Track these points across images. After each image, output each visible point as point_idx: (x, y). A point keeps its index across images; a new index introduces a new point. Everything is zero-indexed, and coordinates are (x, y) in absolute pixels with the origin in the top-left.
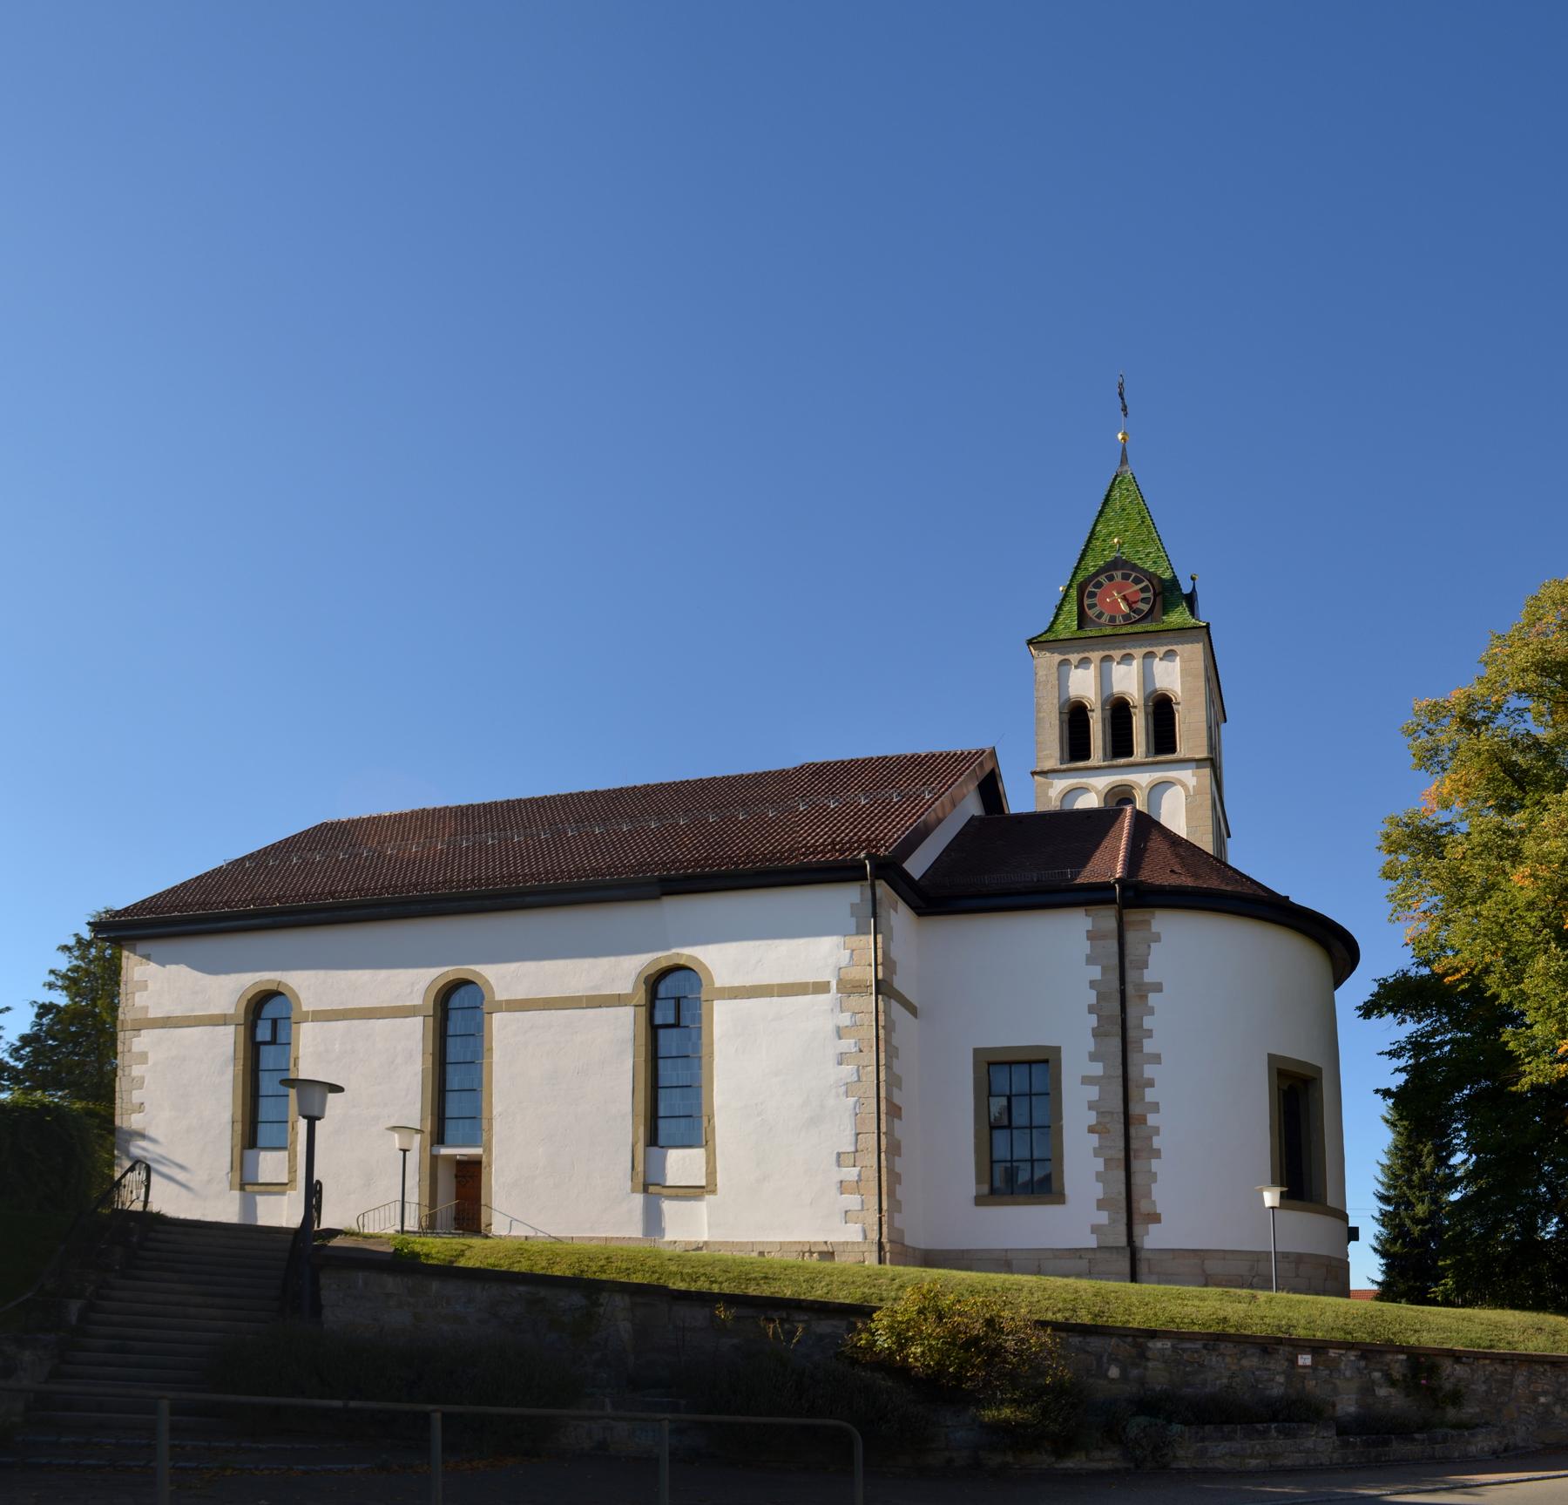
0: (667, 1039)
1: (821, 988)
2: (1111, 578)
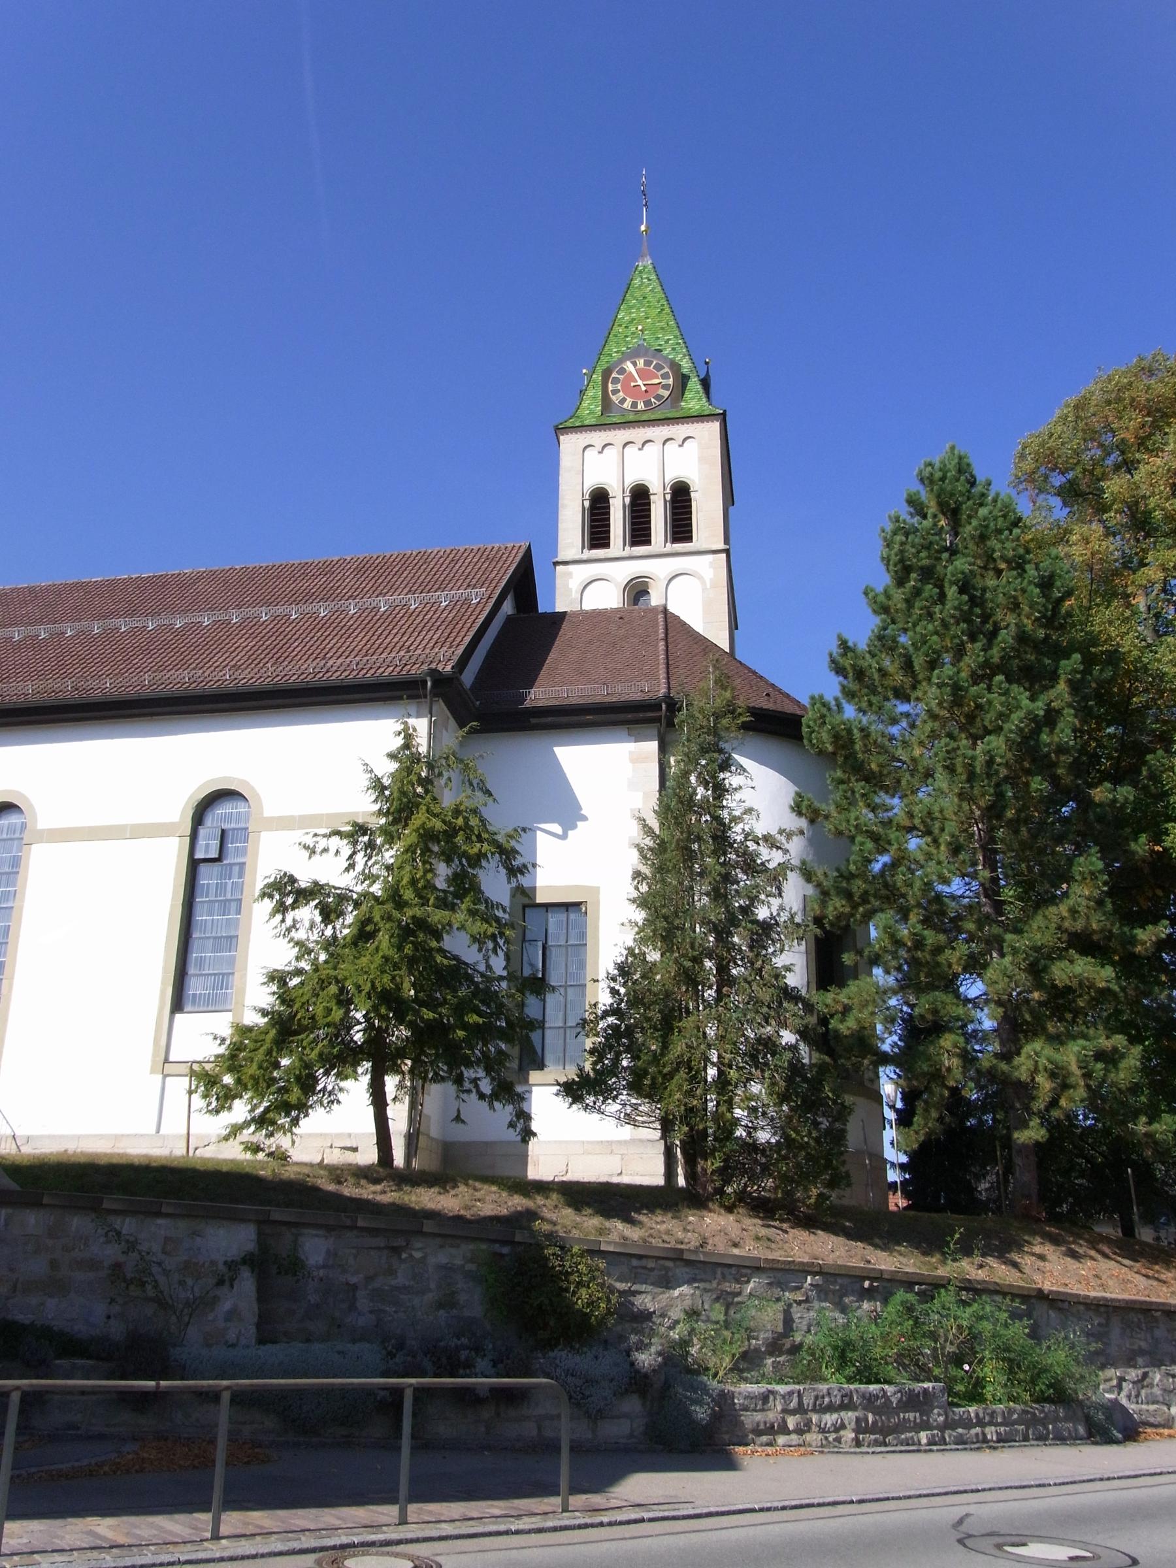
0: (208, 877)
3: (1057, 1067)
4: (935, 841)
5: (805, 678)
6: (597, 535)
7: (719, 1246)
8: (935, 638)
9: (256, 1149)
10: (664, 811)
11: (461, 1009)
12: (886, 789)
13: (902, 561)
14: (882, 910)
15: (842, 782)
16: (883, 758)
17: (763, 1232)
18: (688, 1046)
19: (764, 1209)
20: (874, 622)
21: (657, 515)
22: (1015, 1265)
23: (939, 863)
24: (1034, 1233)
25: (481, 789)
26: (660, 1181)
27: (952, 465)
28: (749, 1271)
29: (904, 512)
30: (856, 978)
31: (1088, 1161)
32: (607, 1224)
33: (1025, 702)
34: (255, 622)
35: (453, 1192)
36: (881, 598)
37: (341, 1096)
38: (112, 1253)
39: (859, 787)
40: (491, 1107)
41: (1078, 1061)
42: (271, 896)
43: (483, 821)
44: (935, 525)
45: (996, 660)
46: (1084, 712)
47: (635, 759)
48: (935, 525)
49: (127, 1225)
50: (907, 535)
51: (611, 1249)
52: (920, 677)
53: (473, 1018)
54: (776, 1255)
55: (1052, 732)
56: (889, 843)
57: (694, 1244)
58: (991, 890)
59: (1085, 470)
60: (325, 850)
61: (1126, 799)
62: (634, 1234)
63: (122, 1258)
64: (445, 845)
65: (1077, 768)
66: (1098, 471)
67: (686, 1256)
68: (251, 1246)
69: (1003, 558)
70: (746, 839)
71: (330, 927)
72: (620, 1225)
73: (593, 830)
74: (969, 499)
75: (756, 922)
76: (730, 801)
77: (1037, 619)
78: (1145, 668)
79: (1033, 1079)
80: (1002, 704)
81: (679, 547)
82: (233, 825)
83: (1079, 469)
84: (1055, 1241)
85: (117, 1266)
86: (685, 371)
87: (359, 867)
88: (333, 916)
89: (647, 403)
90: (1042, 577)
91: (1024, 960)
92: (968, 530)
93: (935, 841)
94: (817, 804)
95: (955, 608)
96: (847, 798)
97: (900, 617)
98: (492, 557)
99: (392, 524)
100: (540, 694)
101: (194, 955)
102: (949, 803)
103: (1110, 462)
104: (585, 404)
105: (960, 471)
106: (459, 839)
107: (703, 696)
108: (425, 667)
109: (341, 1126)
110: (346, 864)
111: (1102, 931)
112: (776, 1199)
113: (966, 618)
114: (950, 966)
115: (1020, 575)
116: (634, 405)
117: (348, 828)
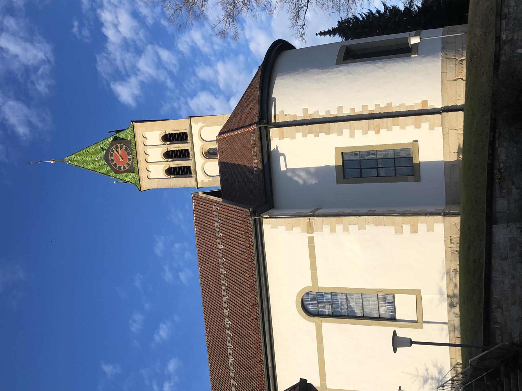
1: (311, 240)
2: (112, 161)
6: (186, 172)
26: (461, 114)
81: (192, 169)
104: (130, 180)
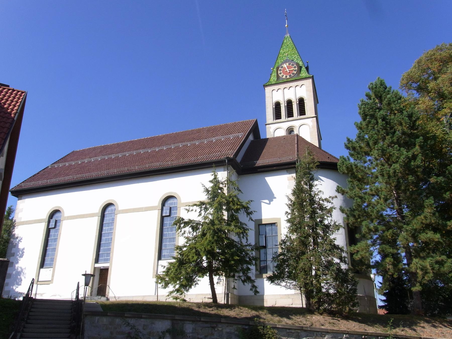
3: (423, 267)
4: (380, 198)
5: (338, 151)
6: (278, 115)
7: (317, 326)
8: (375, 135)
9: (176, 298)
10: (294, 193)
11: (232, 255)
12: (365, 183)
13: (364, 113)
14: (366, 220)
15: (351, 182)
16: (362, 174)
17: (332, 321)
18: (304, 264)
19: (332, 313)
20: (357, 132)
21: (295, 108)
22: (415, 330)
23: (381, 204)
24: (421, 320)
25: (238, 190)
27: (378, 83)
28: (325, 333)
29: (365, 99)
30: (360, 242)
31: (443, 297)
32: (281, 319)
33: (405, 153)
34: (178, 147)
35: (234, 310)
36: (360, 125)
37: (198, 282)
38: (127, 329)
39: (356, 183)
40: (244, 284)
41: (430, 265)
42: (176, 224)
43: (238, 199)
44: (374, 101)
45: (395, 141)
46: (425, 155)
47: (289, 180)
48: (374, 101)
49: (132, 321)
50: (365, 105)
51: (280, 327)
52: (372, 148)
53: (236, 258)
54: (336, 328)
55: (415, 162)
56: (365, 199)
57: (309, 325)
58: (400, 212)
59: (423, 82)
60: (192, 210)
61: (441, 181)
62: (290, 322)
63: (131, 331)
64: (231, 208)
65: (424, 172)
66: (427, 81)
67: (304, 329)
68: (169, 327)
69: (396, 110)
70: (319, 200)
71: (195, 233)
72: (285, 319)
73: (276, 201)
74: (384, 93)
75: (324, 225)
76: (314, 189)
77: (408, 127)
78: (446, 140)
79: (416, 271)
80: (398, 154)
82: (173, 206)
83: (421, 81)
84: (428, 322)
85: (129, 333)
86: (301, 65)
87: (203, 215)
88: (195, 229)
89: (290, 76)
90: (409, 114)
91: (410, 233)
92: (385, 102)
93: (380, 198)
94: (343, 189)
95: (381, 126)
96: (352, 186)
97: (365, 130)
98: (246, 124)
99: (223, 118)
100: (260, 162)
101: (164, 244)
102: (383, 186)
103: (431, 78)
104: (272, 78)
105: (381, 85)
106: (231, 204)
107: (305, 159)
108: (225, 156)
109: (200, 291)
110: (199, 214)
111: (435, 223)
112: (336, 311)
113: (385, 128)
114: (387, 236)
115: (401, 114)
116: (286, 77)
117: (198, 203)
